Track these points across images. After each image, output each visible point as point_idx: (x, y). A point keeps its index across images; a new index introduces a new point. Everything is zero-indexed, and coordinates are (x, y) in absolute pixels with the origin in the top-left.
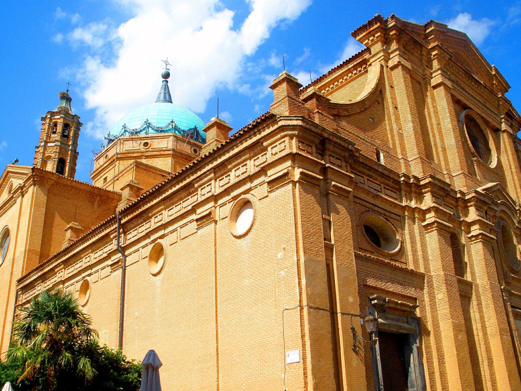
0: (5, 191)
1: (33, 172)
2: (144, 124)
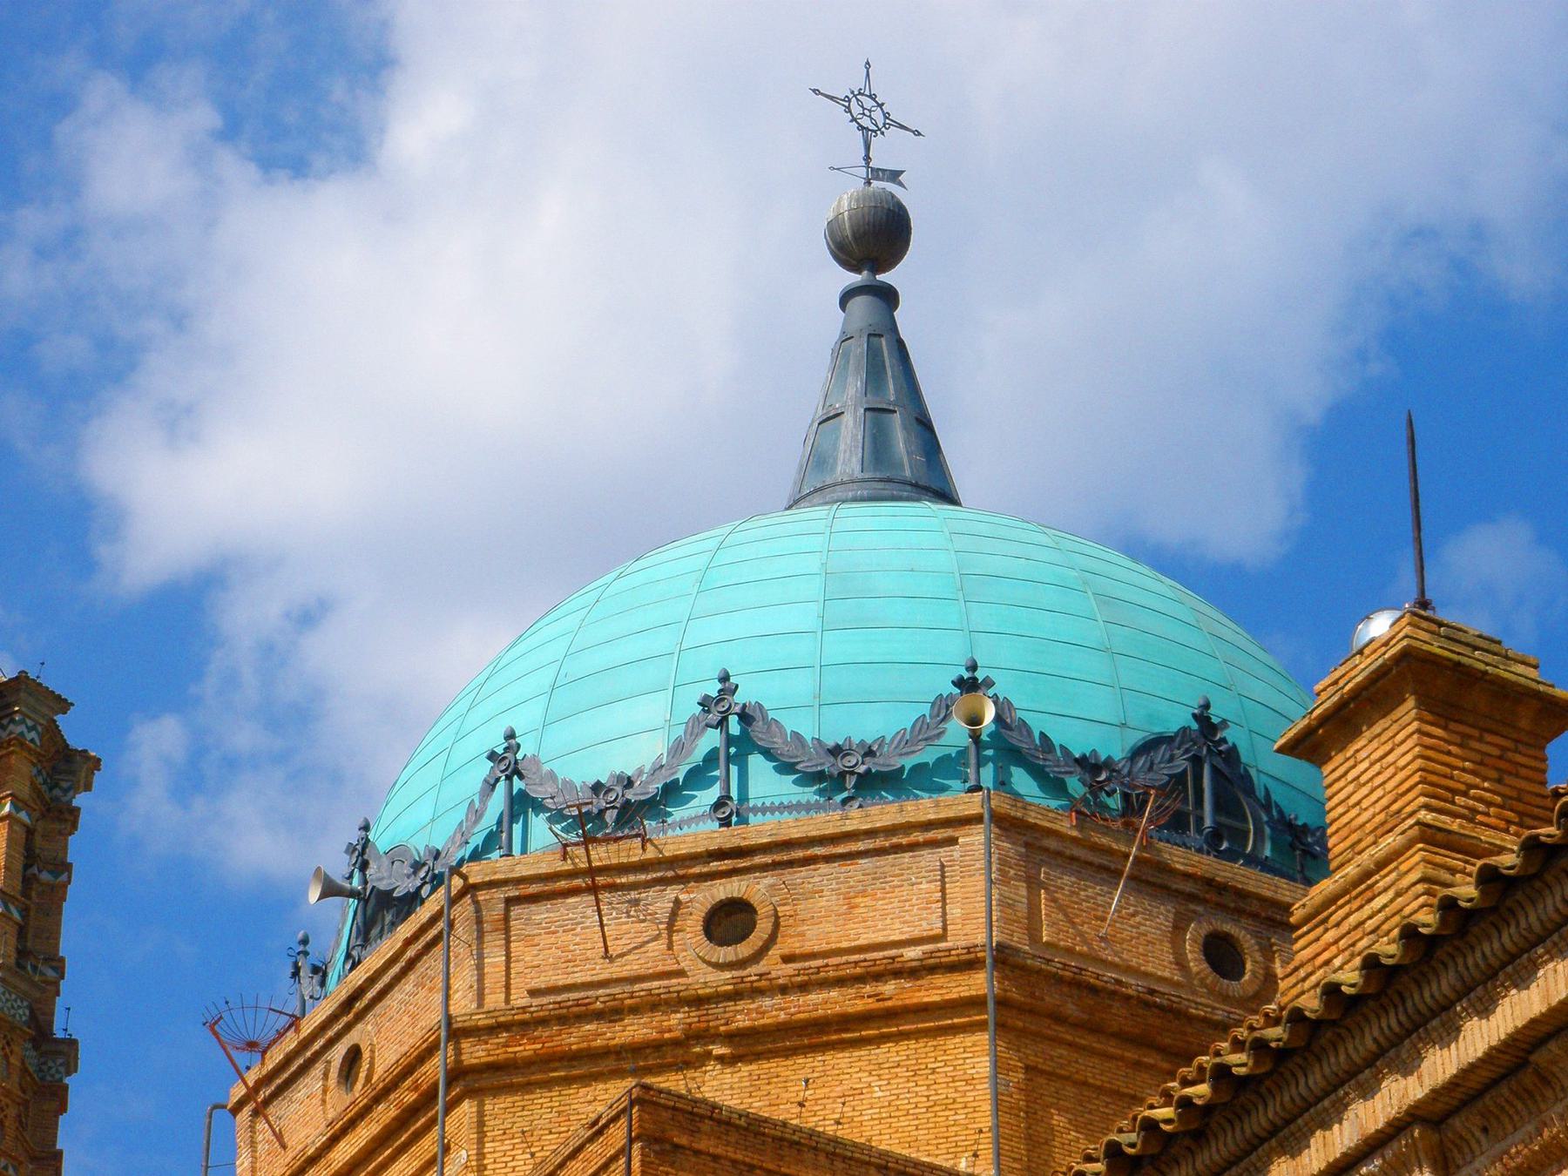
2: (695, 728)
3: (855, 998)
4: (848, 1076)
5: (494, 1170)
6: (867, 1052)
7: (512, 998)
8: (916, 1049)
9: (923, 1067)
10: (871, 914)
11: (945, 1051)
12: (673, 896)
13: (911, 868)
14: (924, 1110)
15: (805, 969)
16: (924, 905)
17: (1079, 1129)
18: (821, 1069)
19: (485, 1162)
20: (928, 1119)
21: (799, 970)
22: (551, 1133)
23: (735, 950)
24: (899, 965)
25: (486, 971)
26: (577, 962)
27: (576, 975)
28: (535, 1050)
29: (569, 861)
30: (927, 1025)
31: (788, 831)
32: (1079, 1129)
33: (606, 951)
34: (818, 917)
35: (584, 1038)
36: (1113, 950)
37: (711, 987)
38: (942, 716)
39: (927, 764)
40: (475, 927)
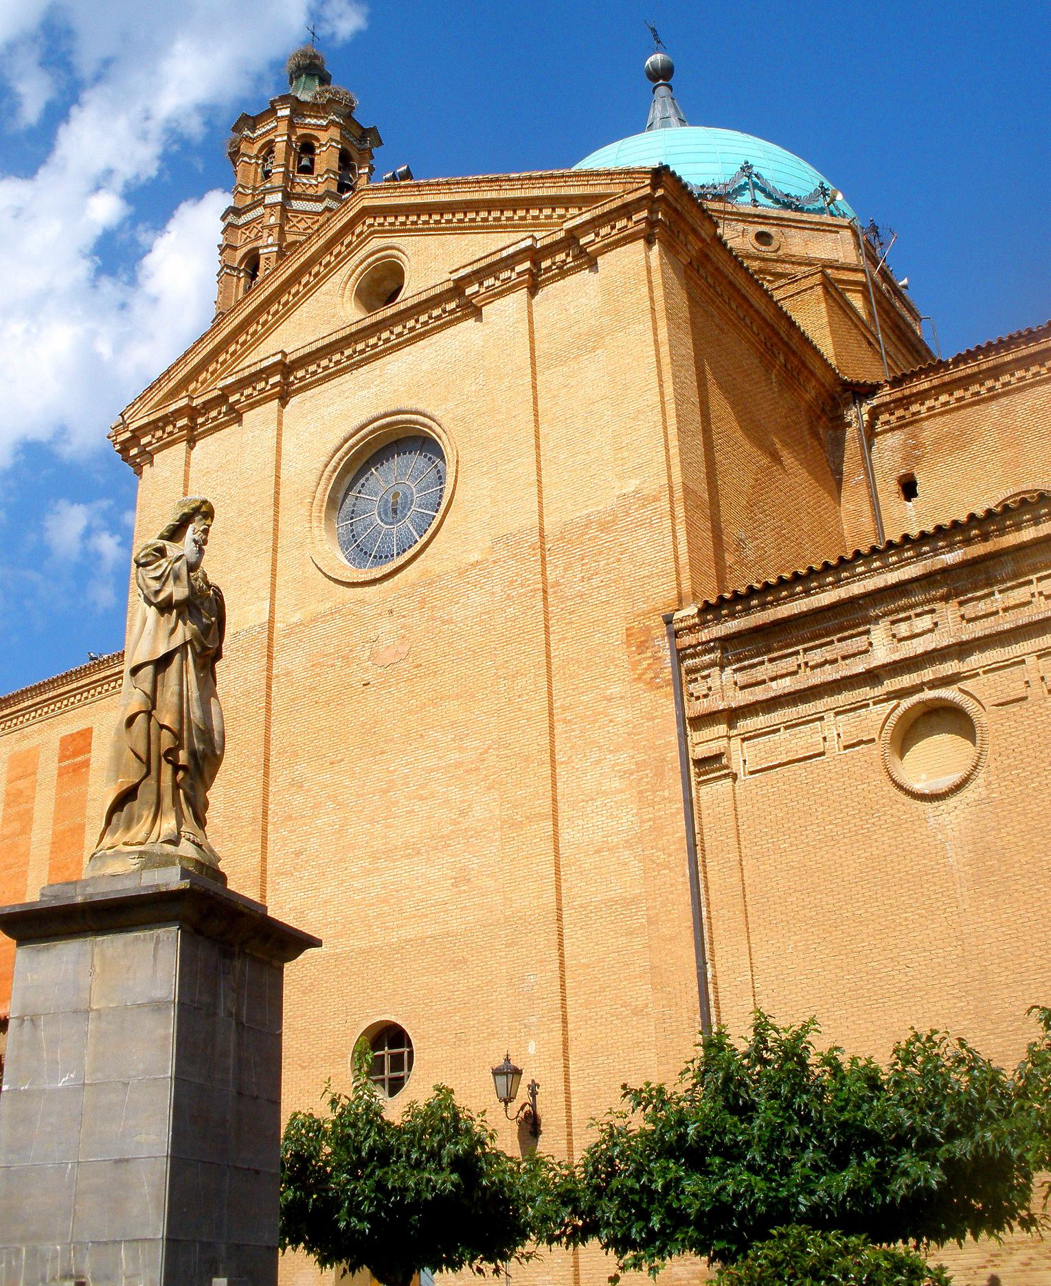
0: (346, 270)
1: (654, 186)
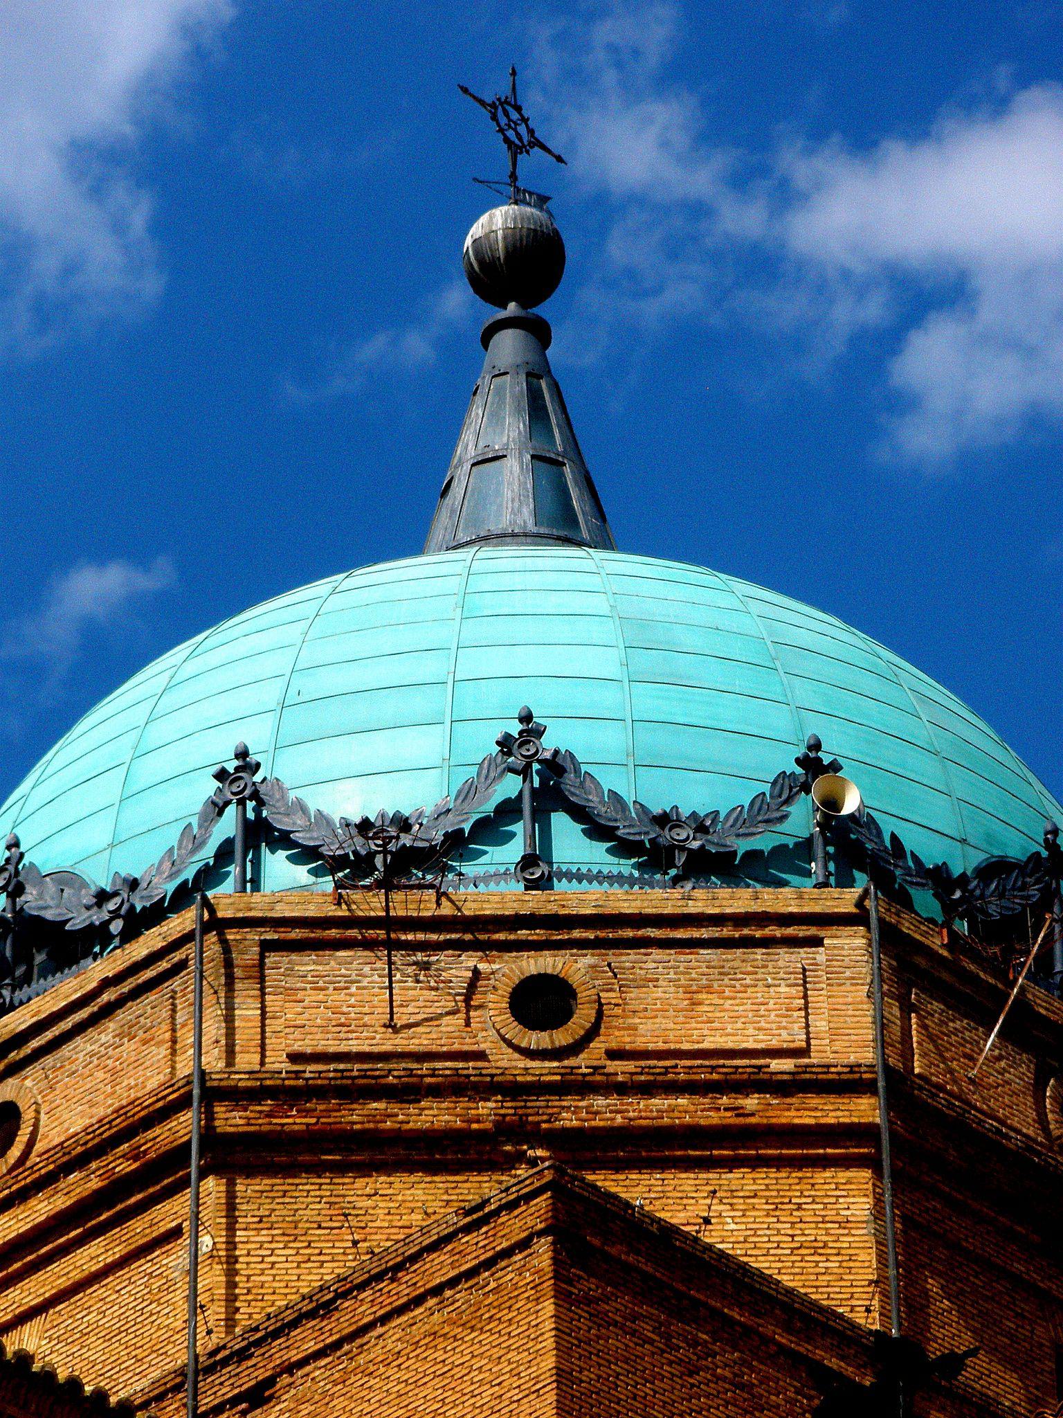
2: (489, 771)
3: (709, 1110)
4: (693, 1201)
5: (248, 1263)
6: (717, 1176)
7: (267, 1060)
8: (777, 1179)
9: (787, 1200)
10: (718, 1014)
11: (813, 1185)
12: (471, 964)
13: (766, 967)
14: (788, 1252)
15: (650, 1067)
16: (784, 1012)
17: (952, 1299)
18: (660, 1189)
19: (237, 1253)
20: (793, 1262)
21: (643, 1068)
22: (320, 1227)
23: (551, 1036)
24: (766, 1077)
25: (237, 1024)
26: (353, 1027)
27: (351, 1042)
28: (308, 1125)
29: (344, 906)
30: (793, 1151)
31: (617, 904)
32: (952, 1299)
33: (392, 1019)
34: (652, 1010)
35: (371, 1117)
36: (982, 1096)
37: (533, 1075)
38: (784, 796)
39: (762, 852)
40: (223, 971)
